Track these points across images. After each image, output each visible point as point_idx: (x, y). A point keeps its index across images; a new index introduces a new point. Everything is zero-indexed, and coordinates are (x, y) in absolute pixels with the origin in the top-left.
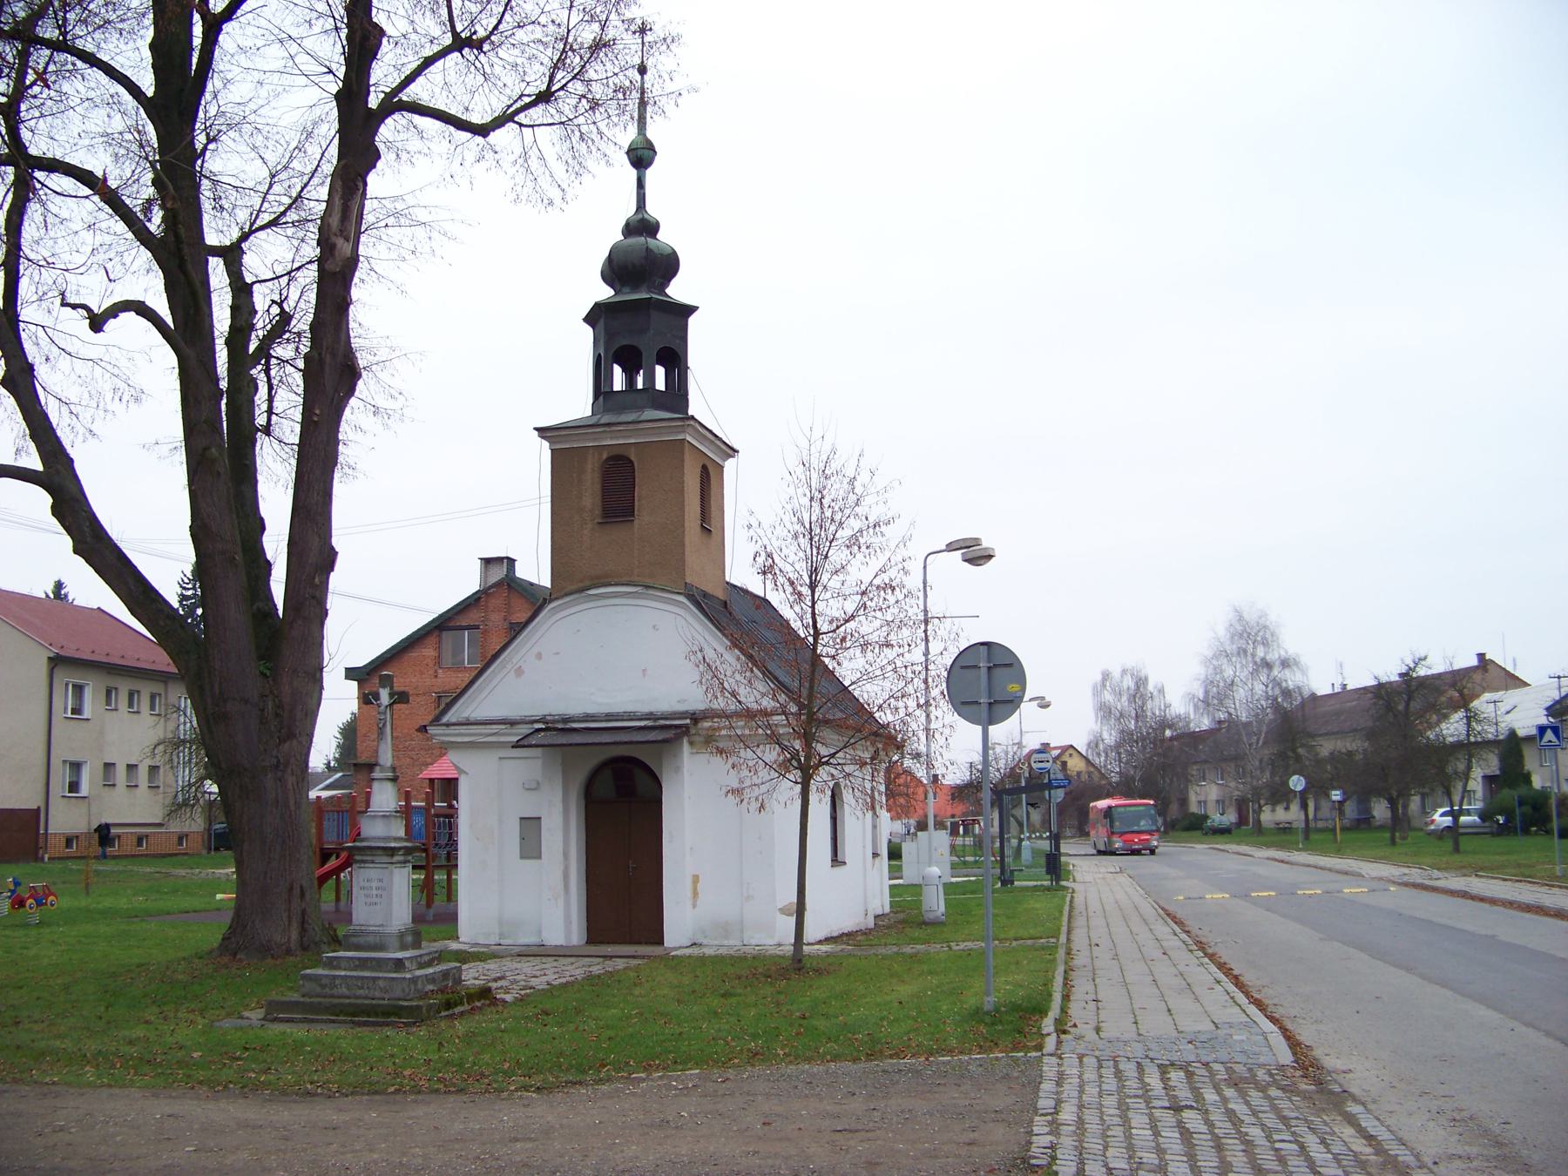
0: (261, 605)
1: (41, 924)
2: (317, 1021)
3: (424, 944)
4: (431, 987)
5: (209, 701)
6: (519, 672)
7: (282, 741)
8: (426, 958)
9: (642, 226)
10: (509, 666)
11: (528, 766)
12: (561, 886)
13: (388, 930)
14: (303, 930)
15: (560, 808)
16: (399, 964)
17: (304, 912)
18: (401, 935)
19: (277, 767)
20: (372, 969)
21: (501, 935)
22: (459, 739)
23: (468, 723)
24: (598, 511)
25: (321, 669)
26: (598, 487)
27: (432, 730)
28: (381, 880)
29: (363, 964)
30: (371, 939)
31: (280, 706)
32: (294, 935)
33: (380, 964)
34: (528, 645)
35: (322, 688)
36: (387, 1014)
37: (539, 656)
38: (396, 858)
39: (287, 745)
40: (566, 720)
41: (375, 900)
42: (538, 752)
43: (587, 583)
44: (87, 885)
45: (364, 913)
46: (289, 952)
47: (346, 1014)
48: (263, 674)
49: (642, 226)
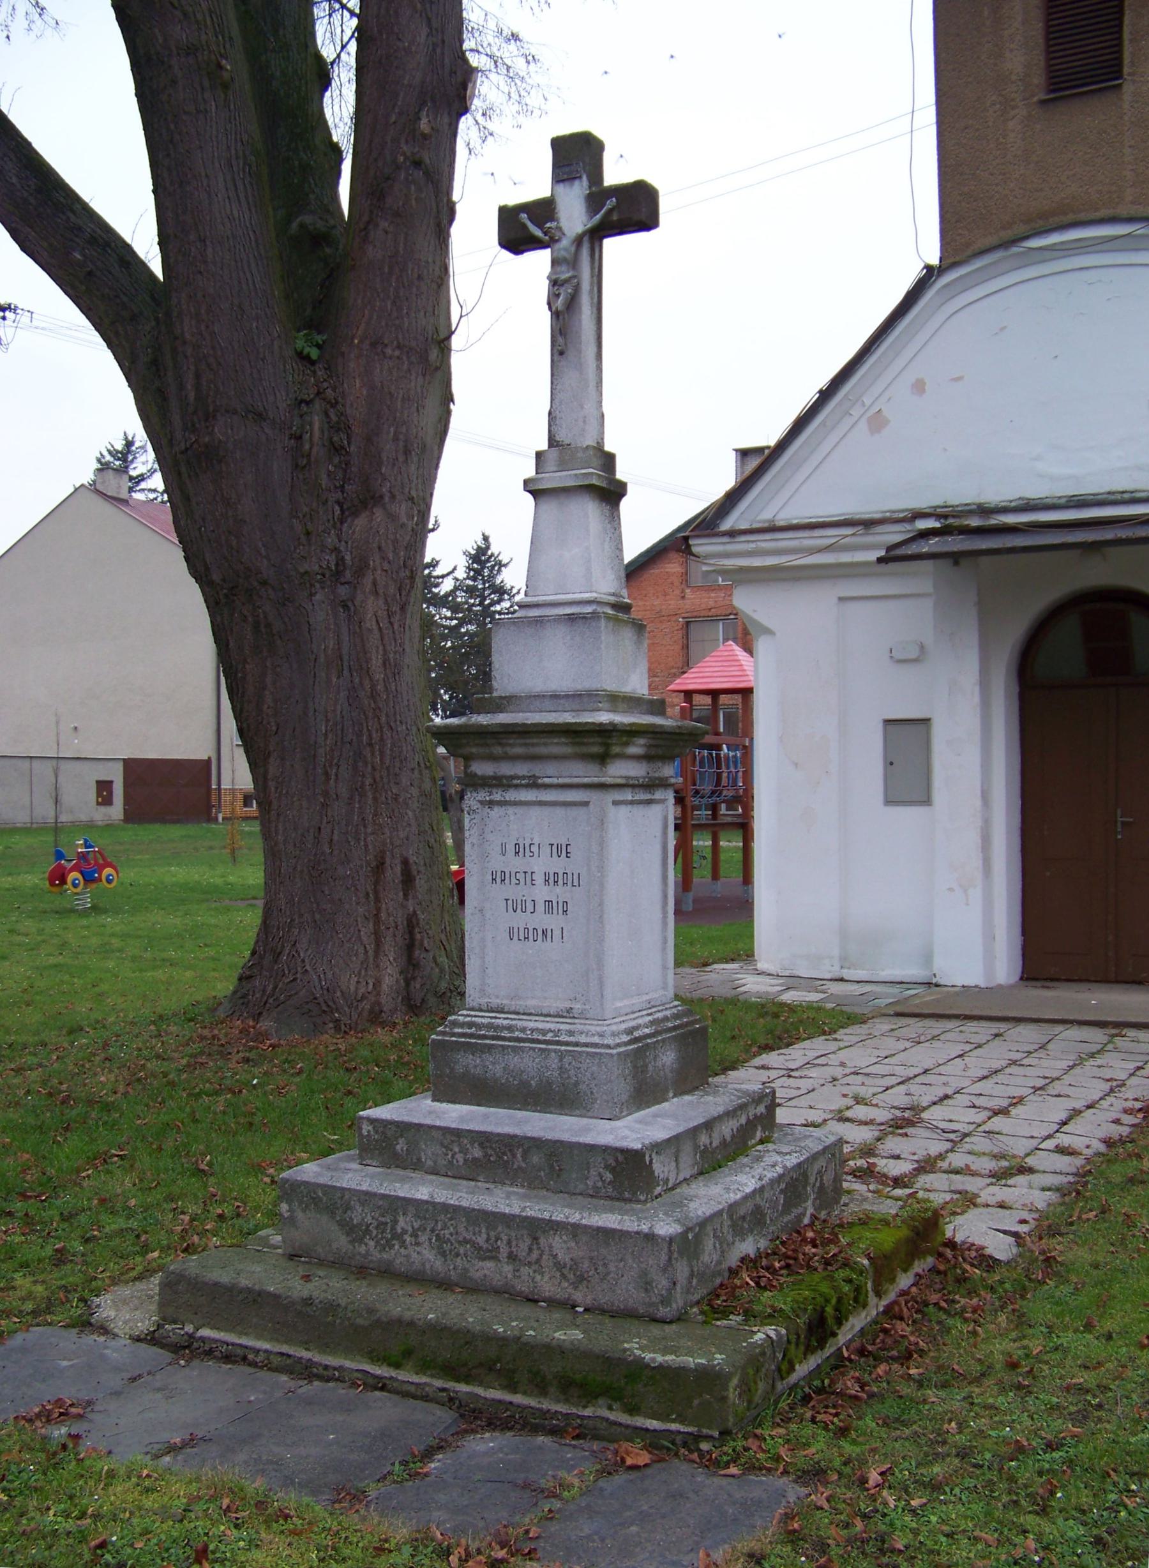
0: (307, 219)
1: (95, 908)
2: (327, 1375)
3: (797, 1367)
4: (748, 1247)
5: (177, 420)
6: (878, 422)
7: (349, 511)
8: (727, 1129)
10: (856, 412)
11: (906, 610)
12: (976, 862)
13: (588, 1032)
14: (411, 966)
15: (977, 699)
16: (629, 1173)
17: (411, 923)
18: (639, 1051)
19: (338, 573)
20: (533, 1182)
21: (844, 961)
22: (757, 562)
23: (772, 529)
24: (1038, 79)
25: (442, 343)
26: (1037, 29)
27: (701, 546)
28: (562, 850)
29: (497, 1158)
30: (527, 1064)
31: (341, 426)
32: (390, 976)
33: (554, 1165)
34: (900, 363)
35: (448, 398)
36: (587, 1392)
37: (919, 387)
38: (618, 770)
39: (361, 522)
40: (984, 510)
41: (541, 920)
42: (928, 565)
43: (1020, 229)
44: (233, 851)
45: (504, 968)
46: (376, 1017)
47: (424, 1367)
48: (302, 357)
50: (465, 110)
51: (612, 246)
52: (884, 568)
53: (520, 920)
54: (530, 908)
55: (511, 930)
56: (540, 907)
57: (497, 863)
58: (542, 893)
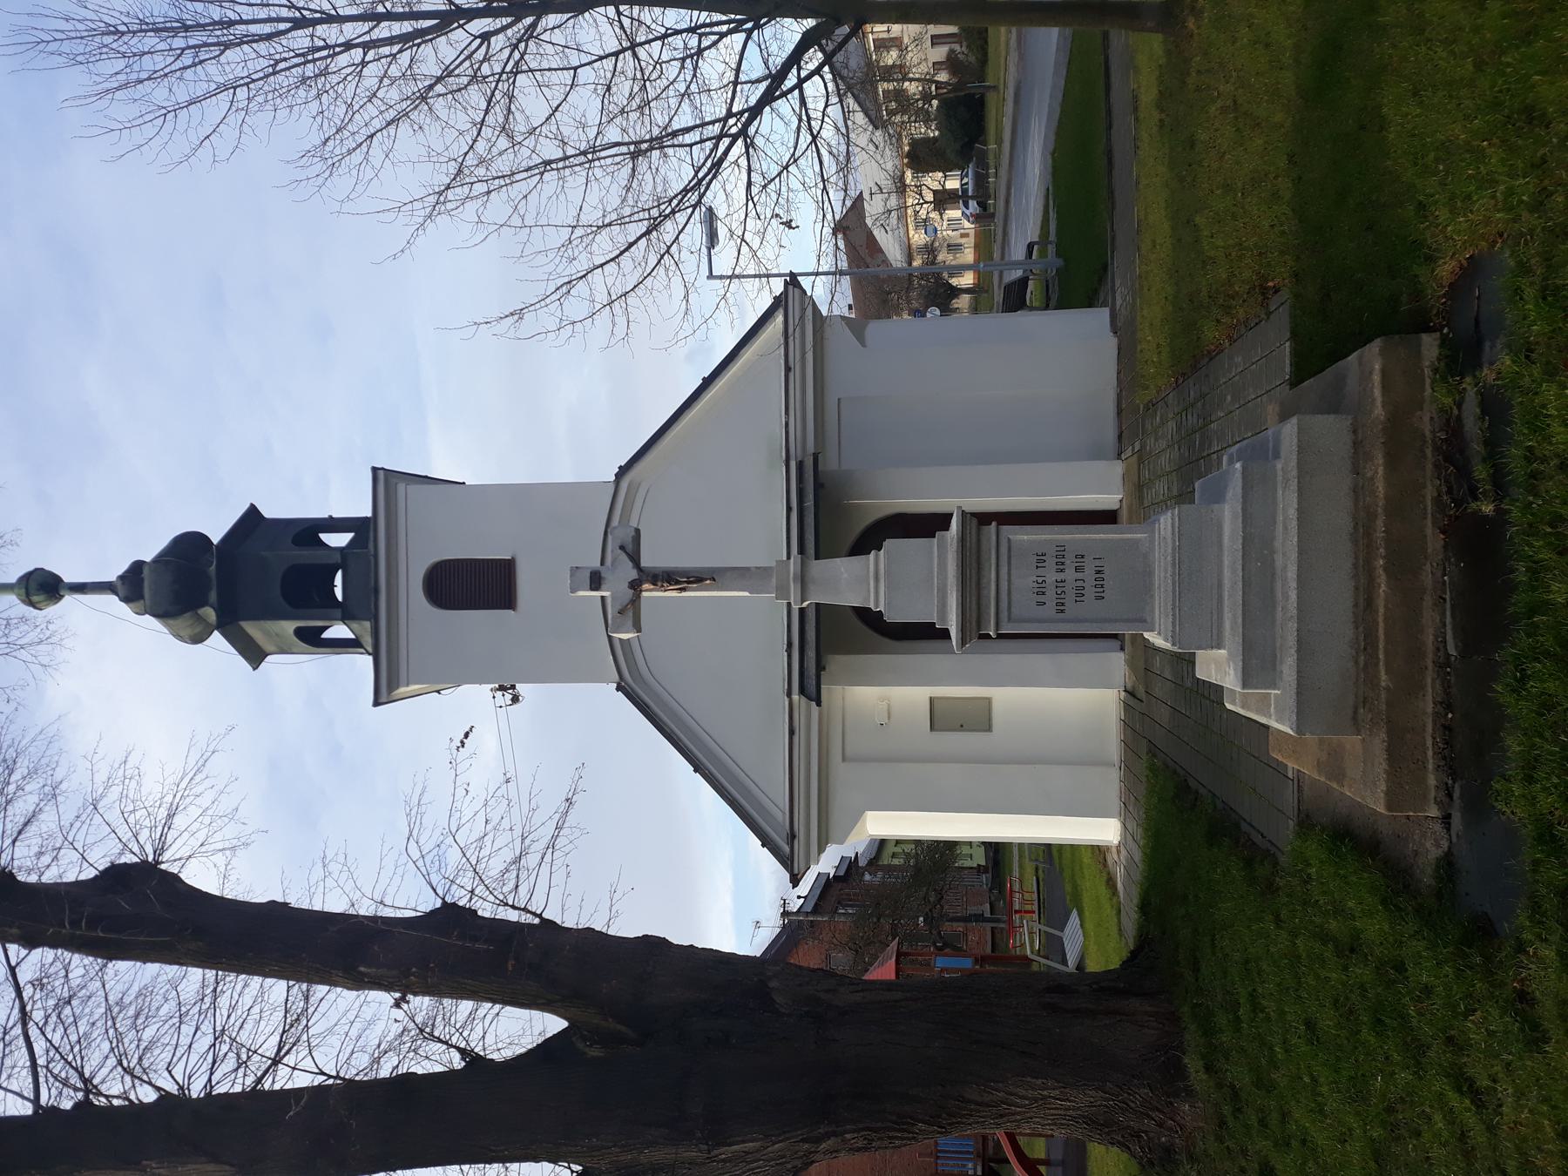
9: (133, 586)
39: (778, 999)
41: (1089, 573)
49: (133, 586)
50: (475, 912)
51: (643, 564)
52: (824, 703)
53: (1090, 592)
54: (1080, 583)
55: (1098, 598)
56: (1080, 575)
57: (1050, 610)
58: (1070, 575)
